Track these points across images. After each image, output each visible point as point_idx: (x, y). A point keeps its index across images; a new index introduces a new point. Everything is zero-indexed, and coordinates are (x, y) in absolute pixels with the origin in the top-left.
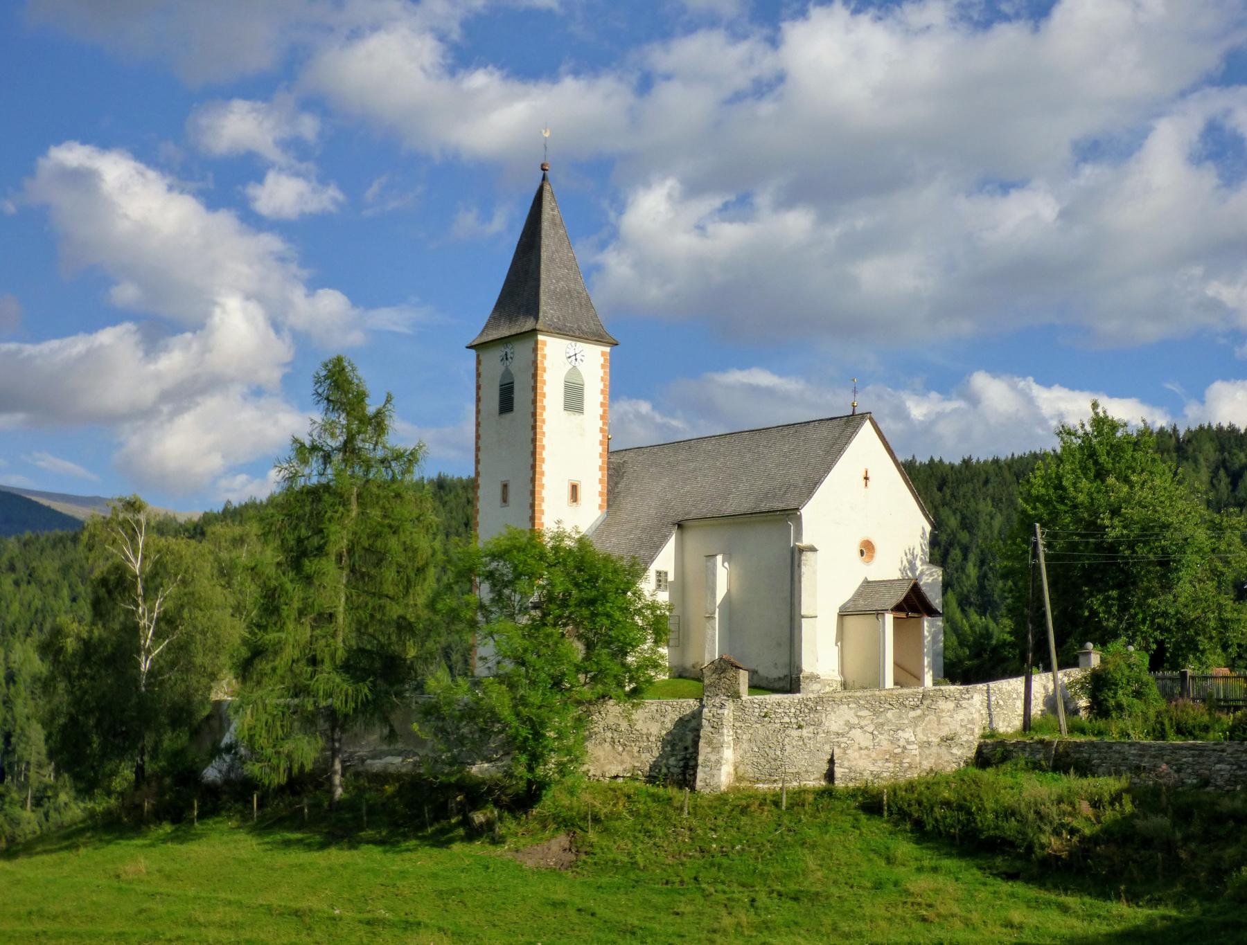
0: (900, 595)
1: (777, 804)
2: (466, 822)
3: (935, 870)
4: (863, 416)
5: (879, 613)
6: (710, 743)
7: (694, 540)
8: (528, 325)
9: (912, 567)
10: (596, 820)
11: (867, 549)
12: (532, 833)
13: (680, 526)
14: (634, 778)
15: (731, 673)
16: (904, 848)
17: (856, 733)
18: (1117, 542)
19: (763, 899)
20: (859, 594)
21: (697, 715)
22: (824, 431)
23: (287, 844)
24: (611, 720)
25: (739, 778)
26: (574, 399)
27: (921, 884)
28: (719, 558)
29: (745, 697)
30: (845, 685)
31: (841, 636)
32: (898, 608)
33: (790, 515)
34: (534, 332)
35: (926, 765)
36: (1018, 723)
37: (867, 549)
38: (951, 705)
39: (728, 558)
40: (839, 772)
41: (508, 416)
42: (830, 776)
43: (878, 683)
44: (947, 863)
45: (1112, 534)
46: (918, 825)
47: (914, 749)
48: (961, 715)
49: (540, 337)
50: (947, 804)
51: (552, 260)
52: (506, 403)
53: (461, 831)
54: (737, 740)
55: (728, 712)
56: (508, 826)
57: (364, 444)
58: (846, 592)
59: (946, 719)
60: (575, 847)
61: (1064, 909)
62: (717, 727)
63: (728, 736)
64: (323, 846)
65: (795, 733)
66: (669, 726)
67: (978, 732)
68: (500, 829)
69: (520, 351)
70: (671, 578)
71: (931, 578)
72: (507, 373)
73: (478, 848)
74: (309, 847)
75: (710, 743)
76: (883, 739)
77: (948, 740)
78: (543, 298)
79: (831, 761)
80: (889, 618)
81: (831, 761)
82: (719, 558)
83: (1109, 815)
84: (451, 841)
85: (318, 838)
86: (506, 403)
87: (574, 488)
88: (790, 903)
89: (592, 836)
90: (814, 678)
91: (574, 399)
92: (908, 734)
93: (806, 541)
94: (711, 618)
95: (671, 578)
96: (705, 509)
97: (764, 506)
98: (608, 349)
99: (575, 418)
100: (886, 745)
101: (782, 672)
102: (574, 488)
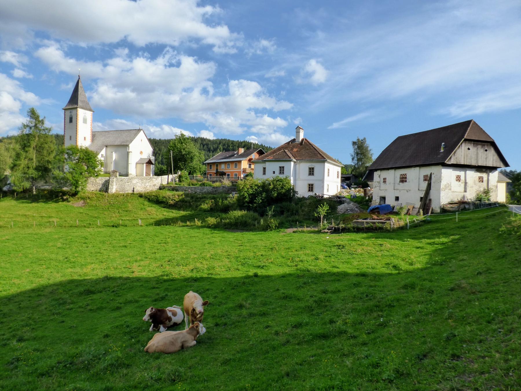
0: (147, 161)
1: (124, 195)
2: (62, 198)
3: (151, 206)
4: (141, 130)
5: (143, 164)
6: (111, 185)
7: (108, 149)
8: (76, 106)
9: (149, 156)
10: (89, 198)
11: (141, 153)
12: (76, 200)
13: (106, 146)
14: (96, 191)
15: (116, 173)
16: (146, 203)
17: (138, 184)
18: (184, 154)
19: (121, 211)
20: (140, 160)
21: (109, 180)
22: (134, 131)
23: (23, 202)
24: (92, 180)
25: (116, 191)
26: (85, 121)
27: (149, 209)
28: (114, 152)
29: (118, 177)
30: (136, 176)
31: (136, 167)
32: (147, 163)
33: (127, 146)
34: (77, 108)
35: (150, 189)
36: (166, 183)
37: (141, 153)
38: (155, 179)
39: (115, 152)
40: (135, 190)
41: (71, 123)
42: (133, 191)
43: (142, 175)
44: (153, 205)
45: (183, 153)
46: (149, 199)
47: (148, 187)
48: (157, 181)
49: (78, 109)
50: (154, 196)
51: (80, 94)
52: (71, 120)
53: (61, 200)
54: (116, 184)
55: (115, 179)
56: (71, 199)
57: (39, 126)
58: (137, 160)
59: (154, 182)
60: (85, 203)
61: (173, 212)
62: (112, 182)
63: (114, 184)
64: (31, 203)
65: (127, 183)
66: (103, 182)
67: (159, 184)
68: (69, 200)
69: (74, 111)
70: (104, 155)
71: (153, 158)
72: (71, 115)
73: (65, 203)
74: (28, 203)
75: (111, 185)
76: (143, 185)
77: (154, 185)
78: (79, 101)
79: (134, 188)
80: (145, 165)
81: (134, 188)
82: (114, 152)
83: (180, 198)
84: (59, 202)
85: (30, 201)
86: (71, 120)
87: (85, 138)
88: (125, 212)
89: (88, 201)
90: (131, 174)
91: (85, 121)
92: (147, 184)
93: (130, 151)
94: (112, 163)
95: (104, 155)
96: (111, 144)
97: (122, 144)
98: (92, 112)
99: (85, 124)
100: (143, 186)
101: (125, 173)
102: (85, 138)
